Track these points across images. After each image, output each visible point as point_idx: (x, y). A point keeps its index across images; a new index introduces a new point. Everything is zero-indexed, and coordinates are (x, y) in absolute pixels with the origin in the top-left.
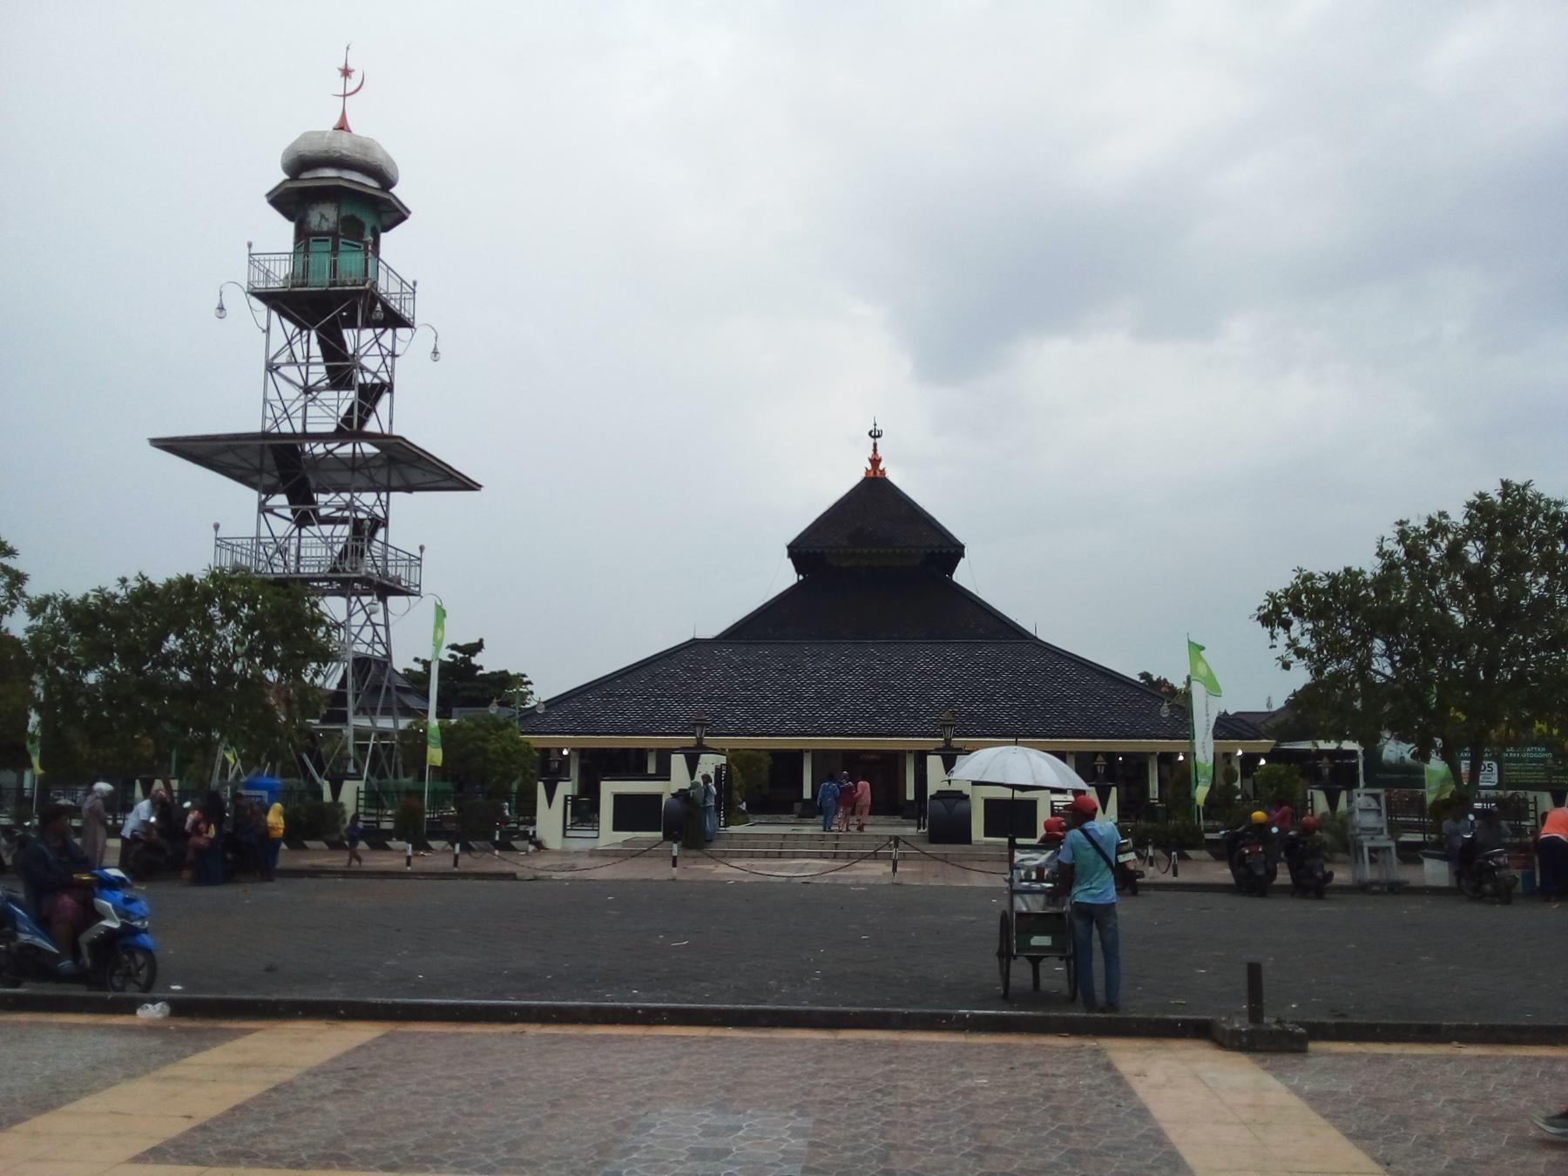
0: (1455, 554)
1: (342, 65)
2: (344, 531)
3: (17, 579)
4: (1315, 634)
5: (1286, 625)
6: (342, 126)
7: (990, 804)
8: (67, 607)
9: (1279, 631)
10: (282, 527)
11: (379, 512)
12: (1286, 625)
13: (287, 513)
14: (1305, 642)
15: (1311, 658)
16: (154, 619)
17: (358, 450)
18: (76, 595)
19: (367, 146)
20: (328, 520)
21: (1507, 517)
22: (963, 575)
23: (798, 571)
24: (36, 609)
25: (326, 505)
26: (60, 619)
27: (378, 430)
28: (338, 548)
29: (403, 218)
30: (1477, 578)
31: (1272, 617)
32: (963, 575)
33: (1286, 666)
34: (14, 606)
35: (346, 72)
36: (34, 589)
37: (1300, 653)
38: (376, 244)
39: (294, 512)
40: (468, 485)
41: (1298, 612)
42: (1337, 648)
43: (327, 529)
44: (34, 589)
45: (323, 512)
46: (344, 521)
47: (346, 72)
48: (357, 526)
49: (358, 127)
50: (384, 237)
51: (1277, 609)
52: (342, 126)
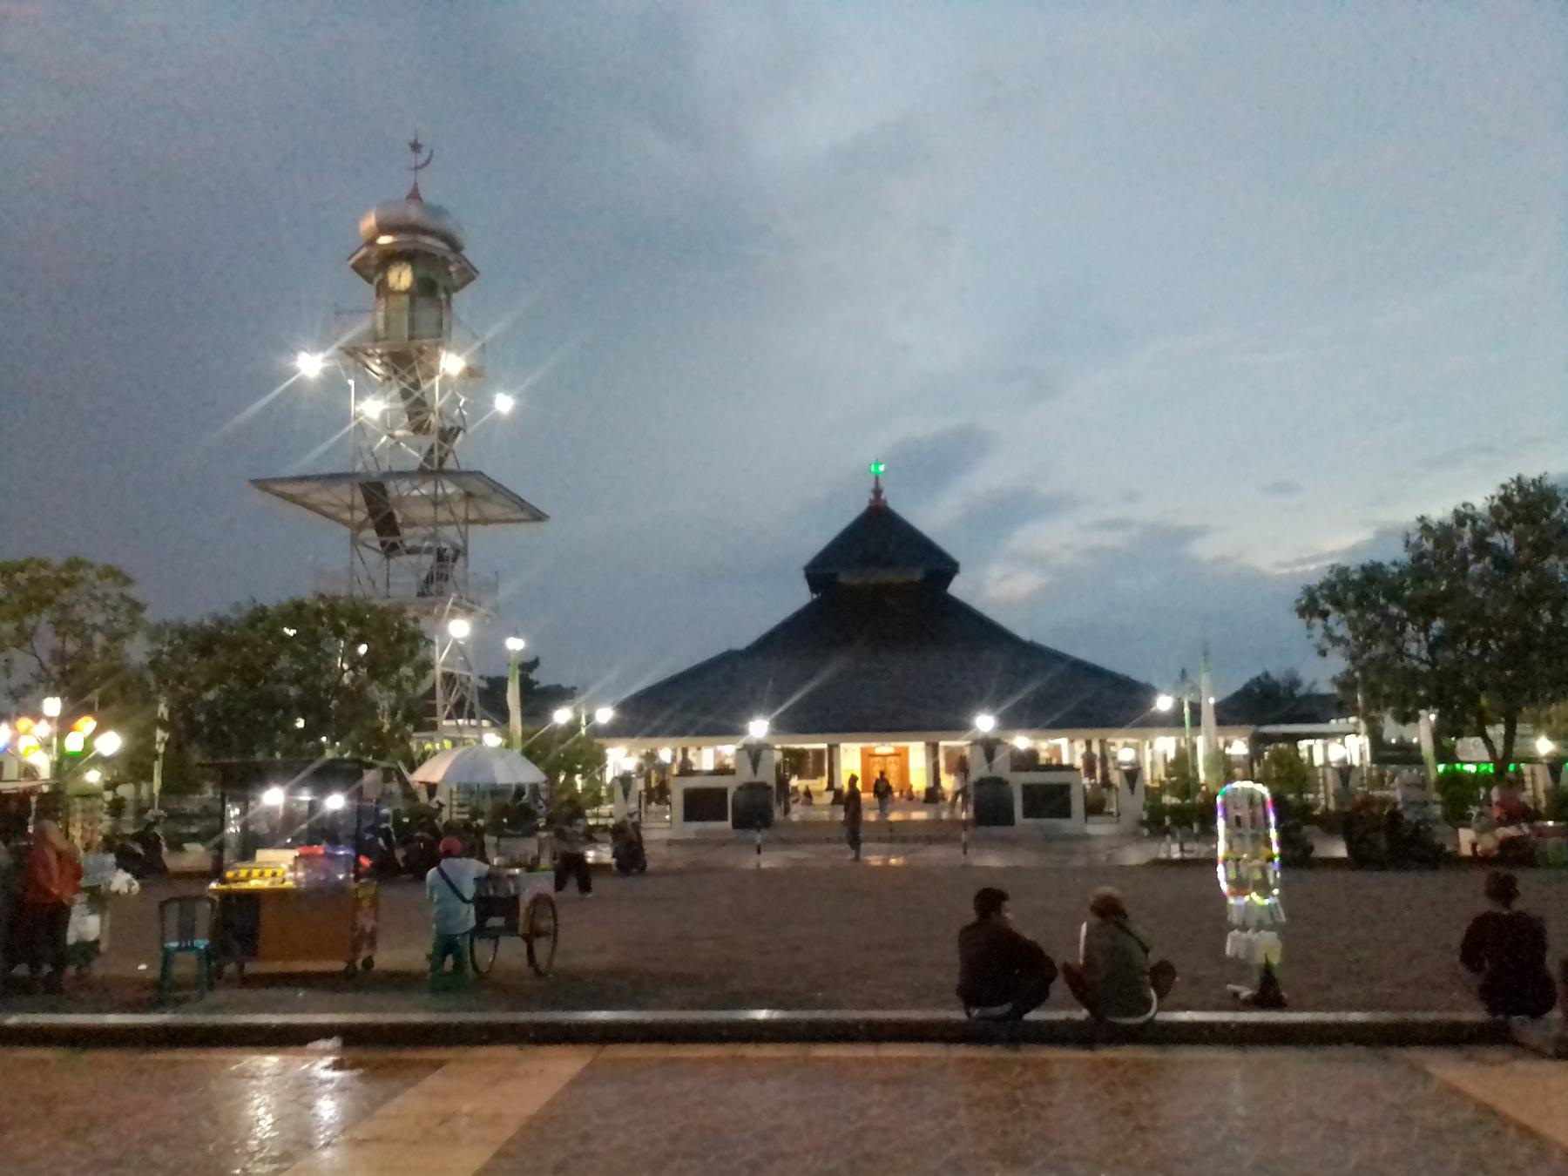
0: (1481, 546)
1: (412, 139)
2: (428, 560)
3: (137, 607)
4: (1353, 626)
5: (1324, 615)
6: (414, 195)
7: (1028, 790)
8: (184, 633)
9: (1318, 622)
10: (373, 557)
11: (460, 542)
12: (1324, 615)
13: (377, 545)
14: (1342, 630)
15: (1347, 643)
16: (361, 639)
17: (440, 491)
18: (191, 620)
19: (439, 212)
20: (412, 551)
21: (1528, 506)
22: (958, 588)
23: (813, 589)
24: (156, 633)
25: (412, 537)
26: (178, 641)
27: (455, 467)
28: (423, 576)
29: (472, 279)
30: (1504, 563)
31: (1310, 607)
32: (958, 588)
33: (1323, 653)
34: (133, 632)
35: (416, 147)
36: (150, 616)
37: (1337, 641)
38: (448, 302)
39: (383, 544)
40: (538, 516)
41: (1339, 604)
42: (1371, 634)
43: (414, 559)
44: (150, 616)
45: (408, 544)
46: (429, 551)
47: (416, 147)
48: (441, 556)
49: (427, 195)
50: (454, 295)
51: (1312, 600)
52: (414, 195)
